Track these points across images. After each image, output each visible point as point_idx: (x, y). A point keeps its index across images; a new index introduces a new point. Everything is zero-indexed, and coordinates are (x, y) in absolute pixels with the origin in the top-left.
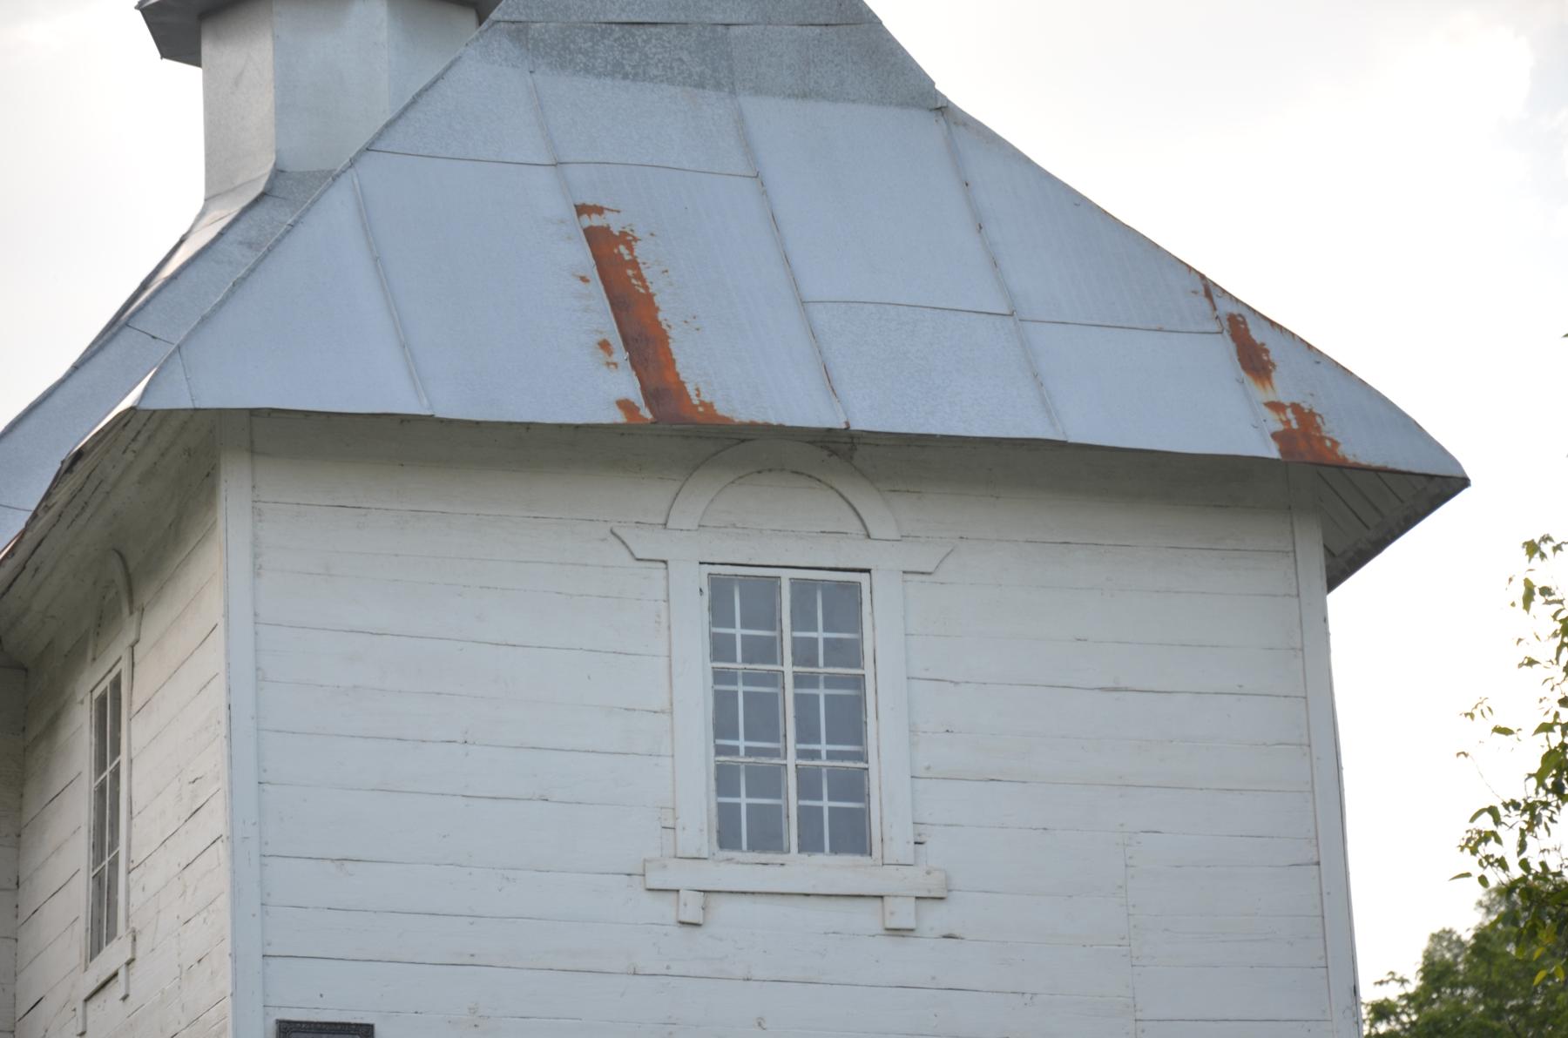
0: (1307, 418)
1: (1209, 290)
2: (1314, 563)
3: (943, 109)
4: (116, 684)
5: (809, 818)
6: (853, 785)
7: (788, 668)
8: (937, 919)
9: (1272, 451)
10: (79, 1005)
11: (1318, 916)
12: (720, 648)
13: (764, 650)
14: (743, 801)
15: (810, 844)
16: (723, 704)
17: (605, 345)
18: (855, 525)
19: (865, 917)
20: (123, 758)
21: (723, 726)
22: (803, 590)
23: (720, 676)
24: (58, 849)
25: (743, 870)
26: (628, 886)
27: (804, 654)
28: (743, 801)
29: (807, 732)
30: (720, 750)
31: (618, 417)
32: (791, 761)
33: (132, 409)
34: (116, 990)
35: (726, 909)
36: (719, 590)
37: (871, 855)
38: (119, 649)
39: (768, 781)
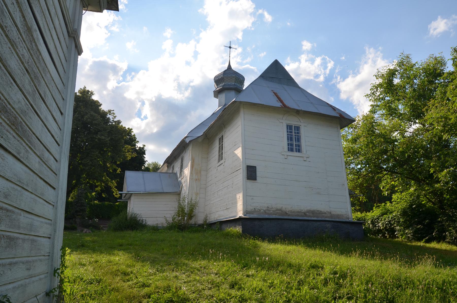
0: (341, 114)
1: (328, 104)
2: (339, 128)
3: (299, 88)
4: (223, 136)
5: (296, 149)
6: (299, 146)
7: (294, 134)
8: (308, 160)
9: (339, 116)
10: (217, 167)
11: (145, 190)
12: (288, 132)
13: (291, 132)
14: (290, 147)
15: (296, 152)
16: (288, 137)
17: (277, 101)
18: (299, 121)
19: (301, 159)
20: (224, 143)
21: (288, 140)
22: (295, 127)
23: (288, 134)
24: (213, 154)
25: (290, 153)
26: (299, 151)
27: (295, 133)
28: (290, 147)
29: (296, 141)
30: (288, 142)
31: (281, 106)
32: (294, 143)
33: (234, 101)
34: (223, 165)
35: (289, 157)
36: (287, 126)
37: (299, 151)
38: (223, 132)
39: (292, 145)
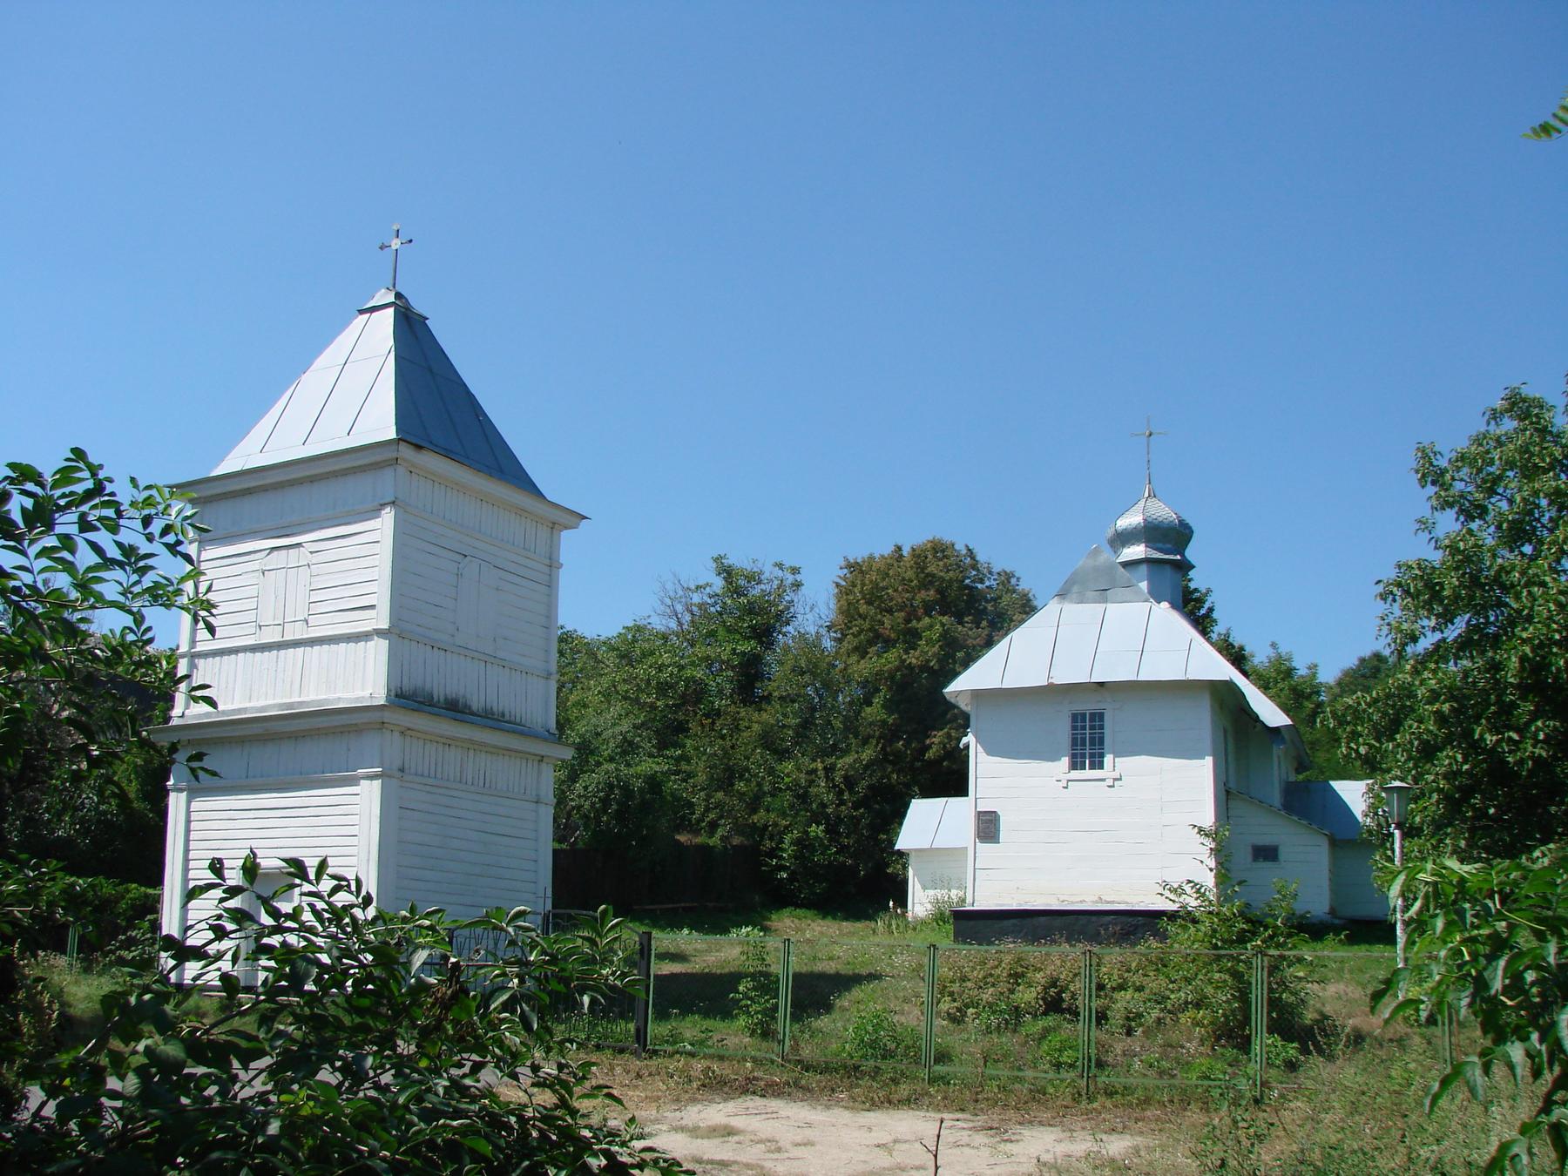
12: (1074, 728)
